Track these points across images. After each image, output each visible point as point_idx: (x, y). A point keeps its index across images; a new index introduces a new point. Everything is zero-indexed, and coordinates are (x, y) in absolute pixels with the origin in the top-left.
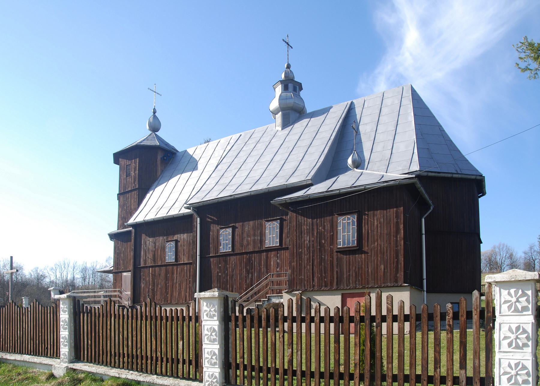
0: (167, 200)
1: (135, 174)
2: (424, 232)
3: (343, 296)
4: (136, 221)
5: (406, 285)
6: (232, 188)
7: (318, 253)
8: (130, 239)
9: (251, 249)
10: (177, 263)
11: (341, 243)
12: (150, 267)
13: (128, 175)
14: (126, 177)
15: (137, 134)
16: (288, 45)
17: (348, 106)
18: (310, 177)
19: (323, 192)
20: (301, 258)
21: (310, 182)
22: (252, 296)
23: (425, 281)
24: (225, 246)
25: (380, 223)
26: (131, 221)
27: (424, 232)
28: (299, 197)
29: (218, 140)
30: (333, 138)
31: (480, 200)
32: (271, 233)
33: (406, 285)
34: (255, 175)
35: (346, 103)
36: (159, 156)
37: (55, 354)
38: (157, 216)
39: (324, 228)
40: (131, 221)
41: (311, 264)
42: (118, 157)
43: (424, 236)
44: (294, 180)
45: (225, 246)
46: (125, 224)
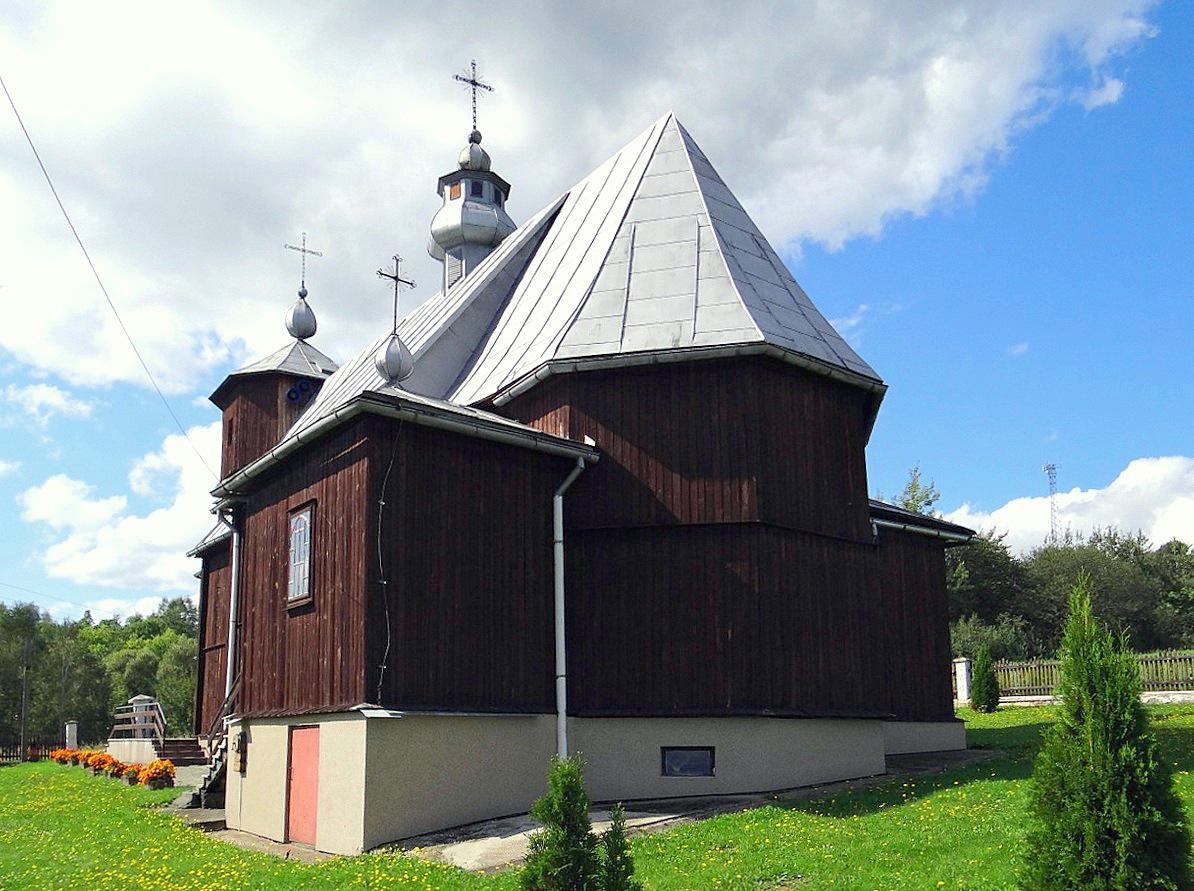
3: (291, 729)
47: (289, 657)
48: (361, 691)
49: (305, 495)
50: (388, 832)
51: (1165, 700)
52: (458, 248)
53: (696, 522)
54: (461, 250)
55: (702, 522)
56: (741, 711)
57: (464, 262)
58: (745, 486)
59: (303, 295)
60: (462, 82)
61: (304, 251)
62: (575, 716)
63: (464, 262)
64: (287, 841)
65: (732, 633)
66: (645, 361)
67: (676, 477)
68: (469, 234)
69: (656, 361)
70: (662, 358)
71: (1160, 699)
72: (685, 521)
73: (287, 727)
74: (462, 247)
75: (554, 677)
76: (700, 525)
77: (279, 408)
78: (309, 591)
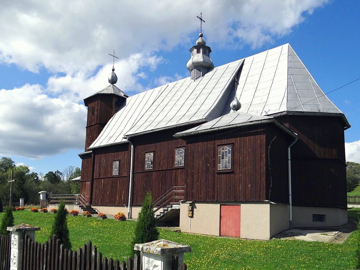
0: (114, 132)
1: (97, 113)
2: (290, 158)
3: (221, 205)
4: (94, 146)
5: (267, 201)
6: (155, 124)
7: (205, 173)
8: (93, 157)
9: (165, 168)
10: (120, 176)
11: (221, 167)
12: (102, 178)
13: (93, 114)
14: (92, 115)
15: (100, 85)
16: (201, 20)
17: (241, 63)
18: (204, 117)
19: (207, 129)
20: (193, 177)
21: (204, 120)
22: (161, 203)
23: (291, 196)
24: (148, 166)
25: (248, 152)
26: (92, 146)
27: (290, 158)
28: (191, 132)
29: (243, 59)
30: (226, 87)
31: (346, 132)
32: (179, 157)
33: (267, 201)
34: (194, 109)
35: (240, 60)
36: (114, 100)
37: (6, 238)
38: (108, 143)
39: (209, 156)
40: (92, 146)
41: (200, 181)
42: (88, 102)
43: (290, 161)
44: (194, 119)
45: (148, 166)
46: (88, 149)
47: (217, 184)
48: (265, 197)
49: (232, 140)
50: (277, 232)
51: (357, 207)
52: (199, 68)
53: (322, 158)
54: (200, 69)
55: (323, 158)
56: (339, 207)
57: (201, 73)
58: (334, 151)
59: (113, 70)
60: (198, 18)
61: (114, 56)
62: (293, 206)
63: (201, 73)
64: (220, 235)
65: (331, 187)
66: (312, 115)
67: (317, 146)
68: (204, 65)
69: (315, 115)
70: (317, 114)
71: (355, 207)
72: (319, 157)
73: (220, 205)
74: (201, 68)
75: (288, 195)
76: (322, 158)
77: (113, 105)
78: (231, 167)
